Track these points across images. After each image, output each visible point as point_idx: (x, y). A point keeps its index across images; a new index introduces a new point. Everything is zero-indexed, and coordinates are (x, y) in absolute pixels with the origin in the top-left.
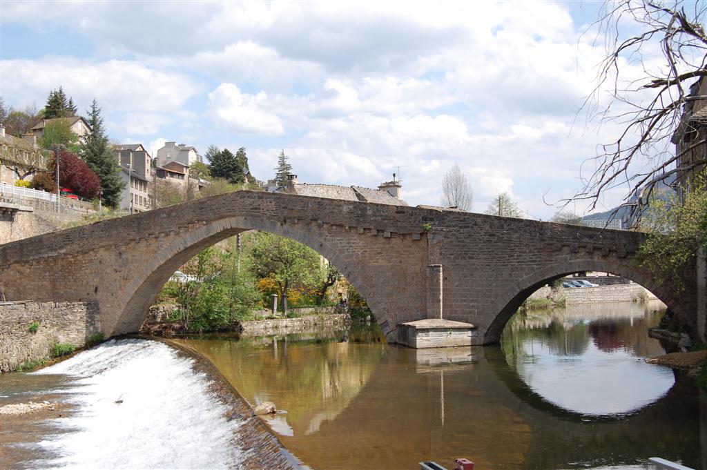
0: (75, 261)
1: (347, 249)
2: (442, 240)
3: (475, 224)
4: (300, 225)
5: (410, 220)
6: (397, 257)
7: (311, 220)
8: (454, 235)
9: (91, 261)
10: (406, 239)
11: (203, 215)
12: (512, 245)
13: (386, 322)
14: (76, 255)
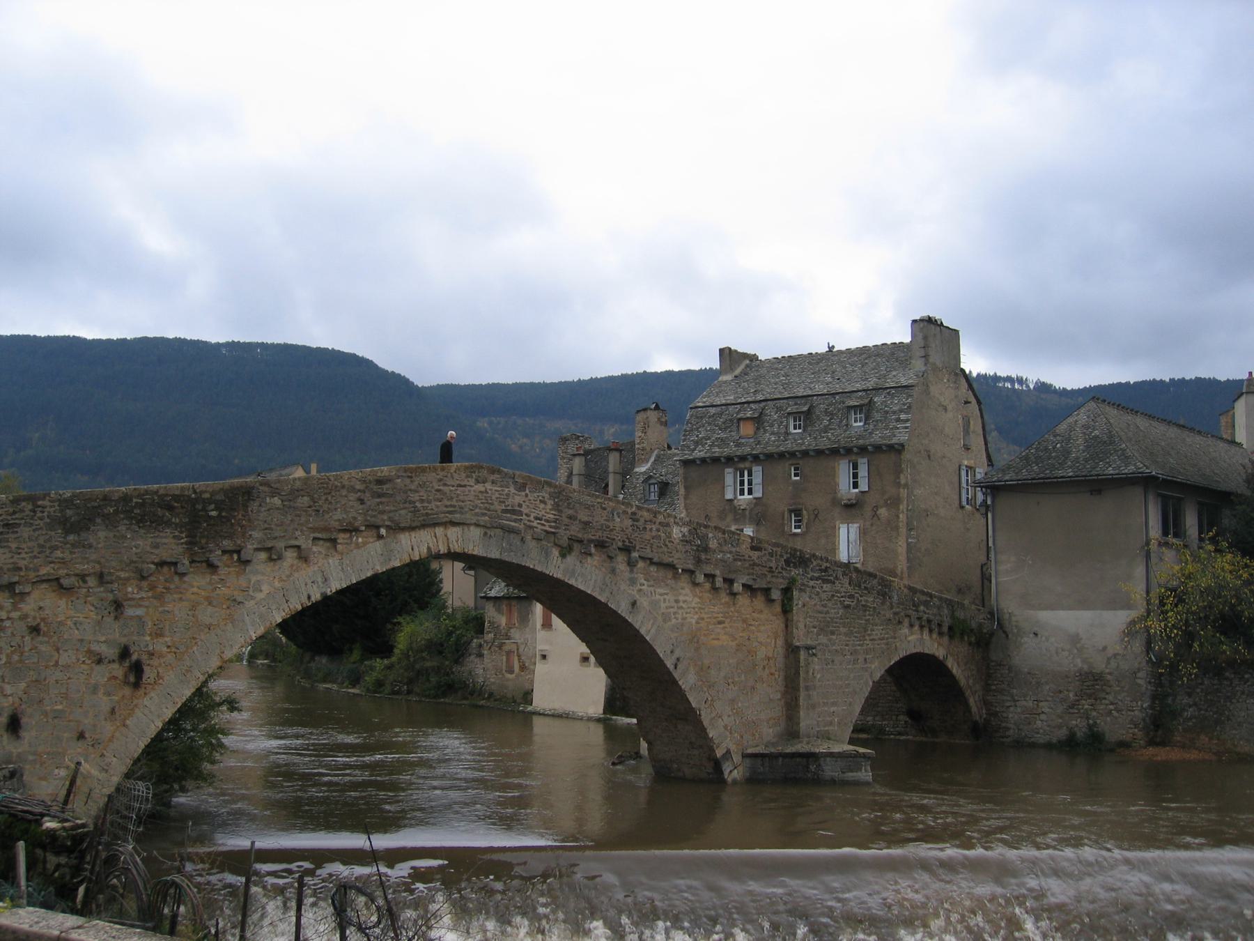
1: (675, 613)
8: (818, 594)
10: (756, 598)
11: (383, 512)
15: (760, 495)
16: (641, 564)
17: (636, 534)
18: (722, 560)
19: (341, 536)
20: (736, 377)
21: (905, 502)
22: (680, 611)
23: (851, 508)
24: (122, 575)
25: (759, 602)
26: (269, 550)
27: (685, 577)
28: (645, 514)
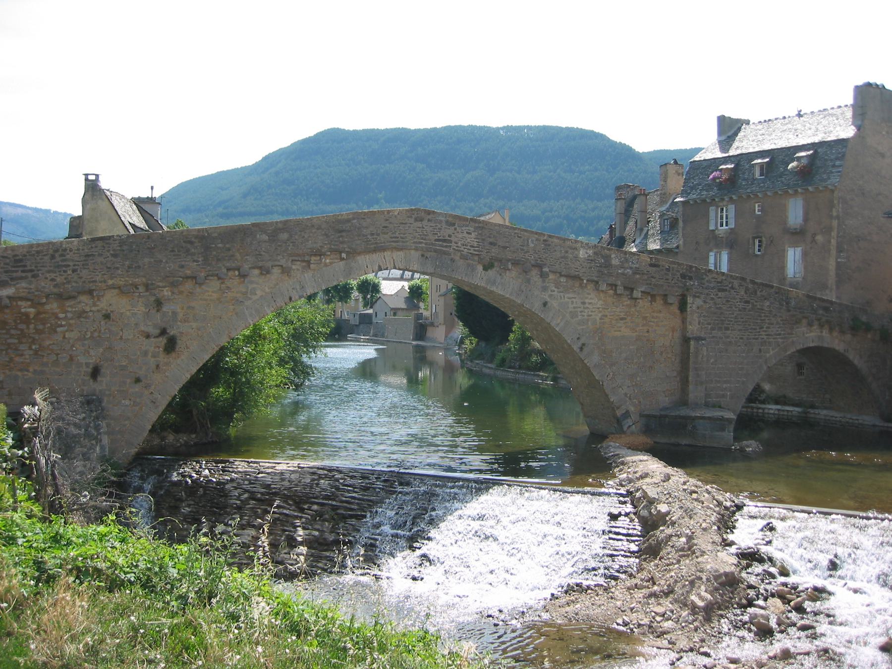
0: (38, 313)
2: (702, 306)
3: (732, 288)
4: (514, 273)
5: (667, 277)
6: (643, 325)
7: (533, 266)
8: (712, 299)
9: (81, 314)
10: (655, 302)
11: (342, 243)
12: (763, 315)
13: (627, 412)
14: (44, 300)
15: (733, 226)
16: (551, 276)
17: (547, 255)
18: (623, 274)
19: (313, 258)
20: (729, 137)
21: (836, 230)
22: (586, 311)
23: (798, 235)
24: (160, 284)
25: (659, 303)
26: (260, 268)
27: (591, 286)
28: (556, 240)
